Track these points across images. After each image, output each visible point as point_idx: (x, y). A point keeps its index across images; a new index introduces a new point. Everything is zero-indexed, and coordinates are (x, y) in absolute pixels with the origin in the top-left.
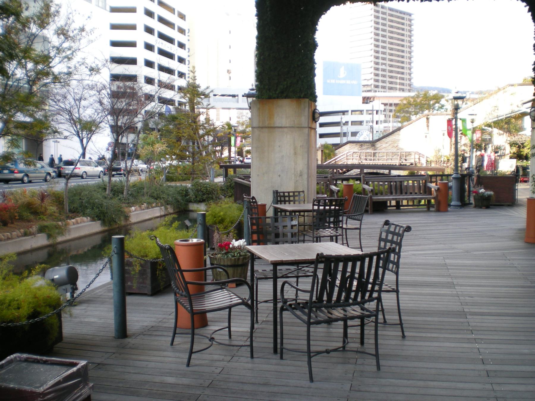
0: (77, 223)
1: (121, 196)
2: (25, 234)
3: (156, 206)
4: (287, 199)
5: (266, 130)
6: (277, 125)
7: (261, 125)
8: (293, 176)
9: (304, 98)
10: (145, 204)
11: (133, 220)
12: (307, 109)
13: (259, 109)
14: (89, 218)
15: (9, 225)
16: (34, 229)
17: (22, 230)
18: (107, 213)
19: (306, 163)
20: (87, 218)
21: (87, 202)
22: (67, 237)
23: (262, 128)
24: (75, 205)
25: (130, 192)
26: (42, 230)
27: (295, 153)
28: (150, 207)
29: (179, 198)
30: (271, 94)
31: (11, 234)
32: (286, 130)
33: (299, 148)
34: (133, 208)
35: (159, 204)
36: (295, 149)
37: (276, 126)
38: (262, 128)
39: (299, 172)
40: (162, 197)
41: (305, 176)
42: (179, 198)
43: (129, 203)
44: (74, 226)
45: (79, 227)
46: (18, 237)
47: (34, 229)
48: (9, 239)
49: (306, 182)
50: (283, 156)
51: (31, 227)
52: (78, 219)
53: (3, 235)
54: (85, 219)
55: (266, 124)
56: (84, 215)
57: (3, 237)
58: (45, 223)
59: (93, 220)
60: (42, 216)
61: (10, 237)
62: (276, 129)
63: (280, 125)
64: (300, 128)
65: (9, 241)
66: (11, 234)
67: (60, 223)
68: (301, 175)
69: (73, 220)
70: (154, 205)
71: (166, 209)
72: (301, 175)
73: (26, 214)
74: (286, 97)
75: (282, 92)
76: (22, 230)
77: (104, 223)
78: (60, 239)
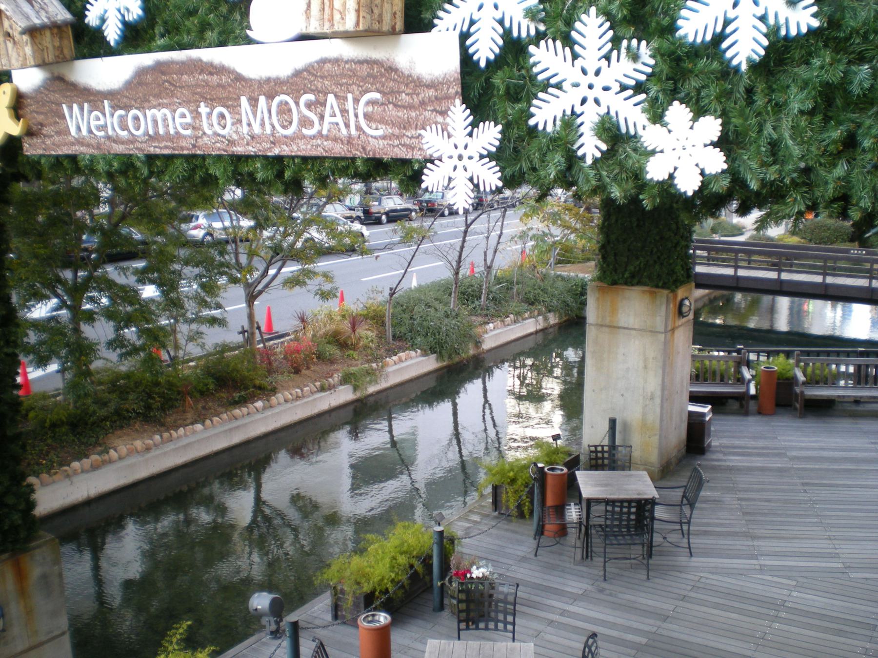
0: (401, 360)
1: (477, 303)
2: (322, 389)
3: (530, 317)
4: (600, 462)
5: (607, 329)
6: (621, 324)
7: (599, 322)
8: (641, 398)
9: (663, 287)
10: (511, 316)
11: (487, 345)
12: (664, 307)
13: (598, 299)
14: (419, 351)
15: (304, 372)
16: (336, 378)
17: (318, 384)
18: (446, 342)
19: (660, 382)
20: (416, 352)
21: (420, 325)
22: (383, 385)
23: (602, 326)
24: (403, 329)
25: (491, 297)
26: (345, 380)
27: (645, 367)
28: (520, 319)
29: (569, 299)
30: (616, 278)
31: (302, 391)
32: (634, 332)
33: (651, 360)
34: (491, 325)
35: (536, 313)
36: (646, 360)
37: (620, 325)
38: (602, 326)
39: (649, 394)
40: (541, 299)
41: (658, 401)
42: (569, 299)
43: (486, 315)
44: (397, 367)
45: (402, 368)
46: (312, 393)
47: (336, 378)
48: (298, 398)
49: (658, 410)
50: (628, 369)
51: (331, 377)
52: (402, 355)
53: (291, 394)
54: (413, 353)
55: (607, 322)
56: (413, 347)
57: (290, 396)
58: (353, 369)
59: (425, 354)
60: (351, 352)
61: (300, 395)
62: (621, 331)
63: (626, 326)
64: (654, 332)
65: (298, 403)
66: (302, 391)
67: (374, 365)
68: (652, 398)
69: (394, 358)
70: (527, 315)
71: (546, 319)
72: (652, 398)
73: (333, 350)
74: (639, 283)
75: (633, 276)
76: (318, 384)
77: (440, 357)
78: (372, 389)
